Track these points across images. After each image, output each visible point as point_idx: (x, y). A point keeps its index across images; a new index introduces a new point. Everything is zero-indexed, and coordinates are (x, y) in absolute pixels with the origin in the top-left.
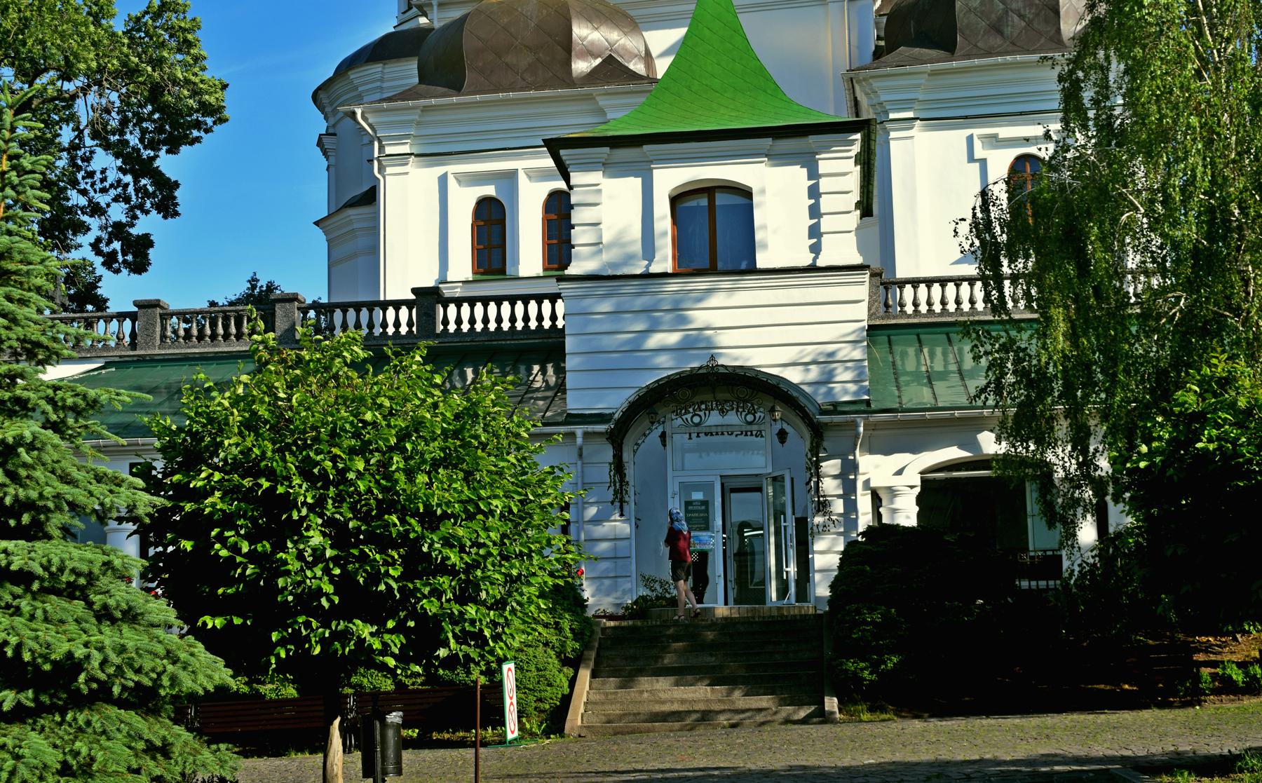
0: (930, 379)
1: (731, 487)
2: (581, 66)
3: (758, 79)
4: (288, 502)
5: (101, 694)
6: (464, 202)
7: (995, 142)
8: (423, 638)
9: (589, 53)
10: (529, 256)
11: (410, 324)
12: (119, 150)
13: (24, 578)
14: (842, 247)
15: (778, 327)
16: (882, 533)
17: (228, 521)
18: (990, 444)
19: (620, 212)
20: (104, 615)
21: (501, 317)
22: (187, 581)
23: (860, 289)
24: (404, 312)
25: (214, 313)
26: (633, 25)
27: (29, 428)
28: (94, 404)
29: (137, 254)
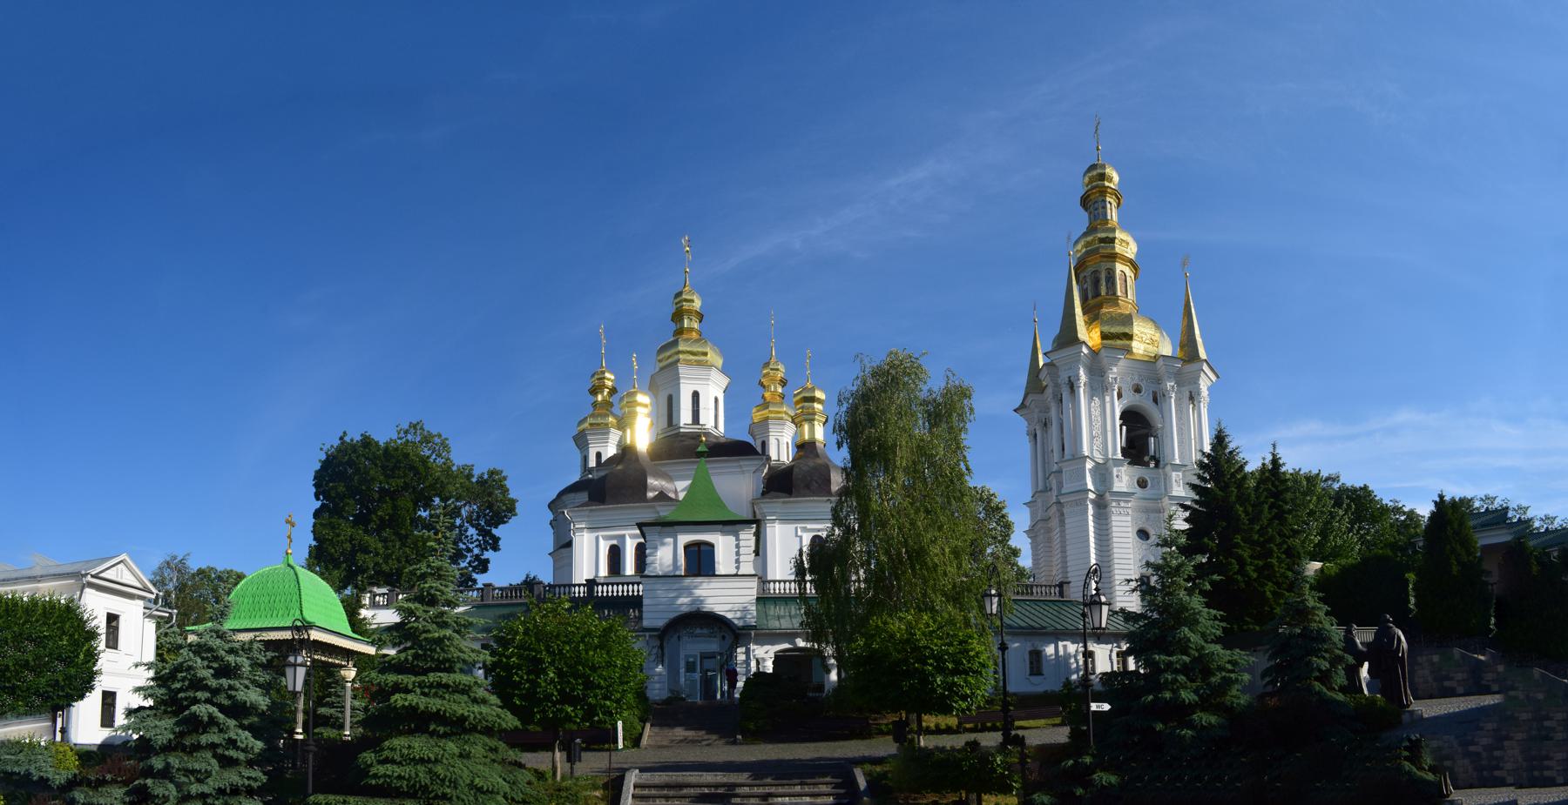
0: (779, 618)
1: (704, 656)
2: (650, 495)
3: (719, 503)
4: (541, 661)
5: (473, 729)
6: (604, 548)
7: (805, 530)
8: (590, 712)
9: (654, 489)
10: (629, 568)
12: (477, 526)
13: (446, 686)
14: (748, 568)
15: (726, 597)
16: (760, 675)
17: (519, 667)
18: (801, 643)
19: (667, 555)
20: (475, 701)
21: (618, 590)
22: (502, 685)
23: (754, 583)
25: (512, 588)
26: (670, 479)
27: (448, 632)
28: (471, 624)
29: (483, 566)
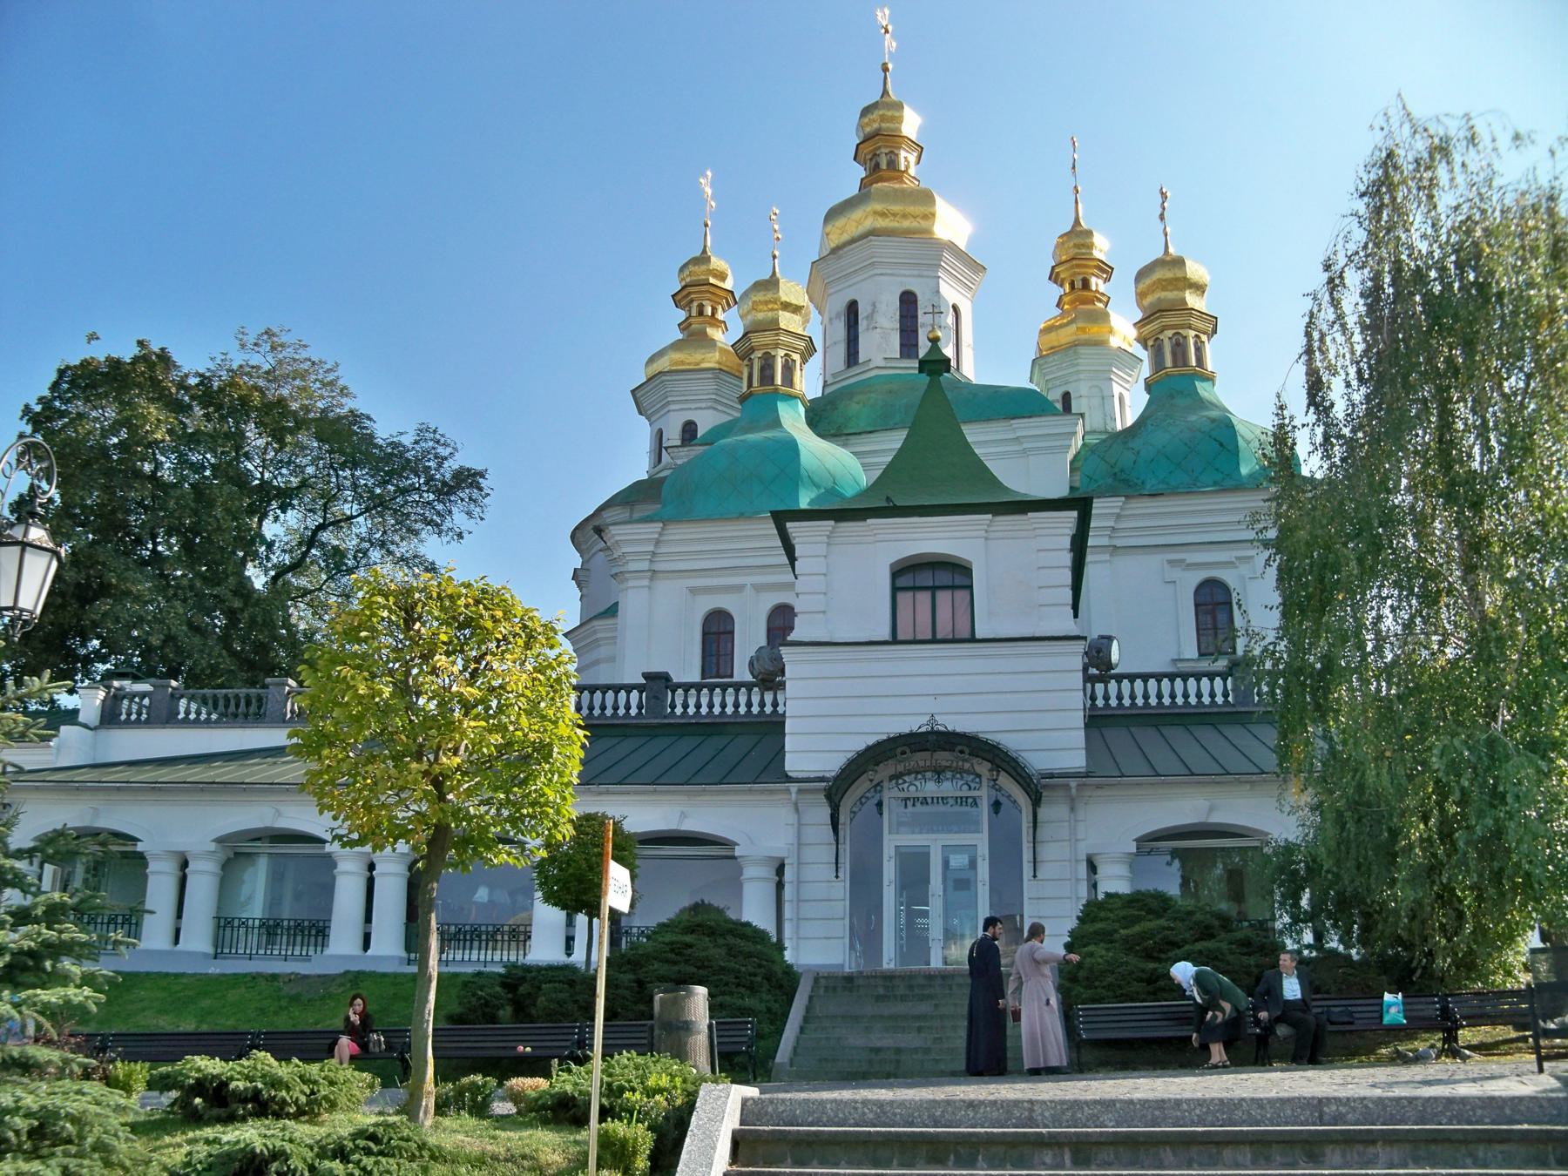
11: (640, 707)
24: (635, 694)
